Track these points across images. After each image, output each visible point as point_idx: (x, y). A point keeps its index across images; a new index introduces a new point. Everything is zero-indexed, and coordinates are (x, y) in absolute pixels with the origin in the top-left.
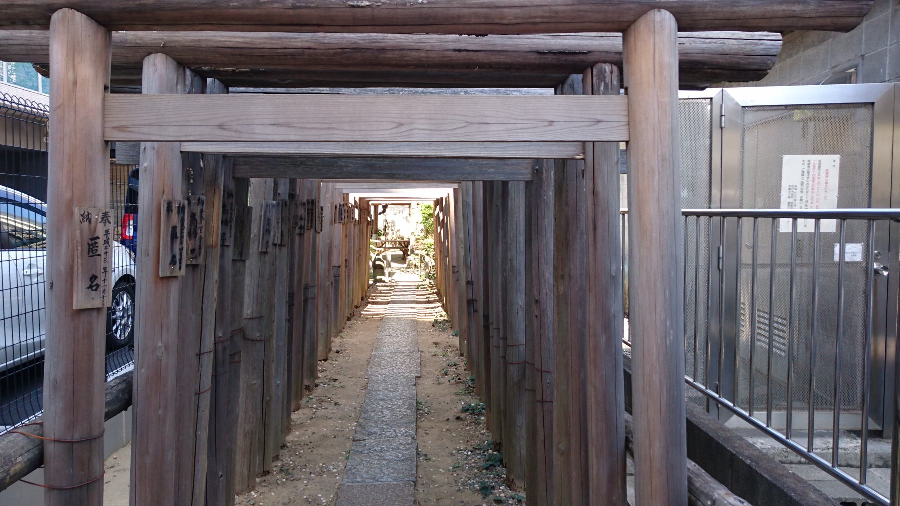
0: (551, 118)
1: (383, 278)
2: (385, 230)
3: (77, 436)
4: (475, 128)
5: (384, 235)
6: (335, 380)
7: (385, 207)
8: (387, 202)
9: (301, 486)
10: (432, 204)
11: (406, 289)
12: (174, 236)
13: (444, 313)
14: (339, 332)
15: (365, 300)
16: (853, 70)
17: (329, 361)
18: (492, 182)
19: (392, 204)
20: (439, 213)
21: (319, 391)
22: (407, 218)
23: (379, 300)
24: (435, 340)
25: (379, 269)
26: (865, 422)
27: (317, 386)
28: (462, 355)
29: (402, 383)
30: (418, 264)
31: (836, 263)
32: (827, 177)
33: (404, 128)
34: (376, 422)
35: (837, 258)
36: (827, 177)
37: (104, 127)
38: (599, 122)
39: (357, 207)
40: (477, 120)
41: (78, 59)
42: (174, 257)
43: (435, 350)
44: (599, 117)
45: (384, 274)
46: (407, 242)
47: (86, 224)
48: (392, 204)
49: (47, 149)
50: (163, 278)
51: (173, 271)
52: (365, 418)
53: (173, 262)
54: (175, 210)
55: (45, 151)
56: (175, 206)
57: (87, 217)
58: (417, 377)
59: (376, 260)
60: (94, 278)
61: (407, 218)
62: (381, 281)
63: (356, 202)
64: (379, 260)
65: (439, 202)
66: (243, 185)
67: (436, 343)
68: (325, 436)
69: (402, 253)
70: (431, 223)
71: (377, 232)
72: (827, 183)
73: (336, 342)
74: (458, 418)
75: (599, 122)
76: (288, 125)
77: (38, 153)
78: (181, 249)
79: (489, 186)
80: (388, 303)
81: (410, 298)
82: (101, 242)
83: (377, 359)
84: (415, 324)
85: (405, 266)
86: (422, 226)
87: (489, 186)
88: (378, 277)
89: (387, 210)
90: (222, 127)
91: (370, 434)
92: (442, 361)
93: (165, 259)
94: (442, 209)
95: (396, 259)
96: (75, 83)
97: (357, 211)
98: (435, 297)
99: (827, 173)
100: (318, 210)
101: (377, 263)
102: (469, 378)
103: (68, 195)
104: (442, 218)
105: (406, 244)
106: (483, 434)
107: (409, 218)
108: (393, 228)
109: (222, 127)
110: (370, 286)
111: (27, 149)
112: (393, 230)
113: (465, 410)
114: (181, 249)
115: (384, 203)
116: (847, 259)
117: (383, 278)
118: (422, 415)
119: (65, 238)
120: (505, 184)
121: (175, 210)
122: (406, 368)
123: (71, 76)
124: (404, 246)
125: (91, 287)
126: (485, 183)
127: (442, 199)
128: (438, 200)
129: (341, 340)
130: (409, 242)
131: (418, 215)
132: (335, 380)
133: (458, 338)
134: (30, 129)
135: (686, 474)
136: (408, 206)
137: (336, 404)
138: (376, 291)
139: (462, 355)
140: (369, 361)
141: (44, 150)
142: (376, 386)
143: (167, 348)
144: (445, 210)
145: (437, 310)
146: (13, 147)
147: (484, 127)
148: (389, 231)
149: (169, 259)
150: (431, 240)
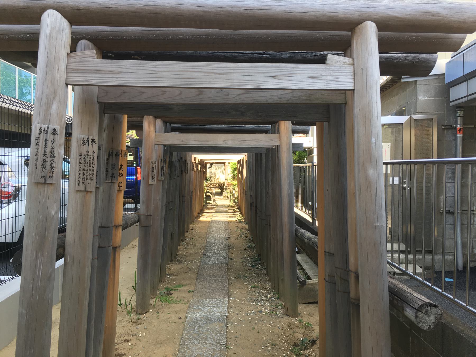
0: (261, 139)
1: (211, 202)
2: (211, 177)
3: (148, 214)
4: (242, 142)
5: (210, 181)
6: (193, 238)
7: (212, 164)
8: (213, 162)
9: (185, 265)
10: (236, 163)
11: (222, 206)
12: (162, 169)
13: (241, 216)
14: (192, 223)
15: (201, 212)
16: (405, 108)
17: (189, 232)
18: (257, 154)
19: (216, 163)
20: (239, 168)
21: (187, 241)
22: (222, 171)
23: (209, 211)
24: (237, 225)
25: (208, 198)
26: (407, 248)
27: (185, 240)
28: (249, 230)
29: (222, 239)
30: (229, 196)
31: (390, 185)
32: (386, 151)
33: (226, 142)
34: (211, 249)
35: (391, 183)
36: (386, 151)
37: (155, 141)
38: (273, 140)
39: (199, 164)
40: (244, 140)
41: (150, 126)
42: (162, 174)
43: (237, 229)
44: (273, 139)
45: (210, 200)
46: (222, 184)
47: (152, 164)
48: (216, 163)
49: (31, 131)
50: (159, 180)
51: (161, 178)
52: (207, 249)
53: (162, 176)
54: (162, 162)
55: (30, 133)
56: (163, 160)
57: (152, 162)
58: (228, 237)
59: (207, 192)
60: (153, 177)
61: (222, 171)
62: (209, 203)
63: (199, 161)
64: (209, 192)
65: (239, 162)
66: (171, 154)
67: (237, 227)
68: (192, 254)
69: (220, 191)
70: (236, 173)
71: (206, 178)
72: (386, 154)
73: (191, 226)
74: (245, 250)
75: (273, 140)
76: (198, 141)
77: (26, 134)
78: (163, 172)
79: (257, 155)
80: (214, 213)
81: (224, 210)
82: (154, 168)
83: (210, 232)
84: (228, 223)
85: (222, 197)
86: (232, 175)
87: (257, 155)
88: (208, 202)
89: (213, 166)
90: (182, 141)
91: (209, 253)
92: (239, 233)
93: (160, 175)
94: (240, 166)
95: (217, 194)
96: (150, 131)
97: (199, 166)
98: (237, 210)
99: (386, 150)
100: (187, 165)
101: (208, 194)
102: (251, 237)
103: (148, 157)
104: (240, 170)
105: (223, 185)
106: (255, 253)
107: (224, 172)
108: (215, 178)
109: (182, 141)
110: (204, 205)
111: (15, 132)
112: (214, 178)
113: (248, 247)
114: (163, 172)
115: (211, 162)
116: (394, 184)
117: (211, 202)
118: (230, 248)
119: (147, 167)
120: (261, 154)
121: (162, 162)
122: (223, 234)
123: (149, 130)
124: (221, 187)
125: (152, 179)
126: (255, 154)
127: (241, 160)
128: (239, 160)
129: (193, 225)
130: (224, 185)
131: (229, 169)
132: (193, 238)
133: (247, 225)
134: (23, 122)
135: (295, 228)
136: (223, 164)
137: (194, 245)
138: (207, 208)
139: (249, 230)
140: (207, 233)
141: (29, 133)
142: (211, 240)
143: (159, 199)
144: (242, 166)
145: (238, 215)
146: (15, 132)
147: (245, 142)
148: (212, 179)
149: (161, 175)
150: (236, 182)
